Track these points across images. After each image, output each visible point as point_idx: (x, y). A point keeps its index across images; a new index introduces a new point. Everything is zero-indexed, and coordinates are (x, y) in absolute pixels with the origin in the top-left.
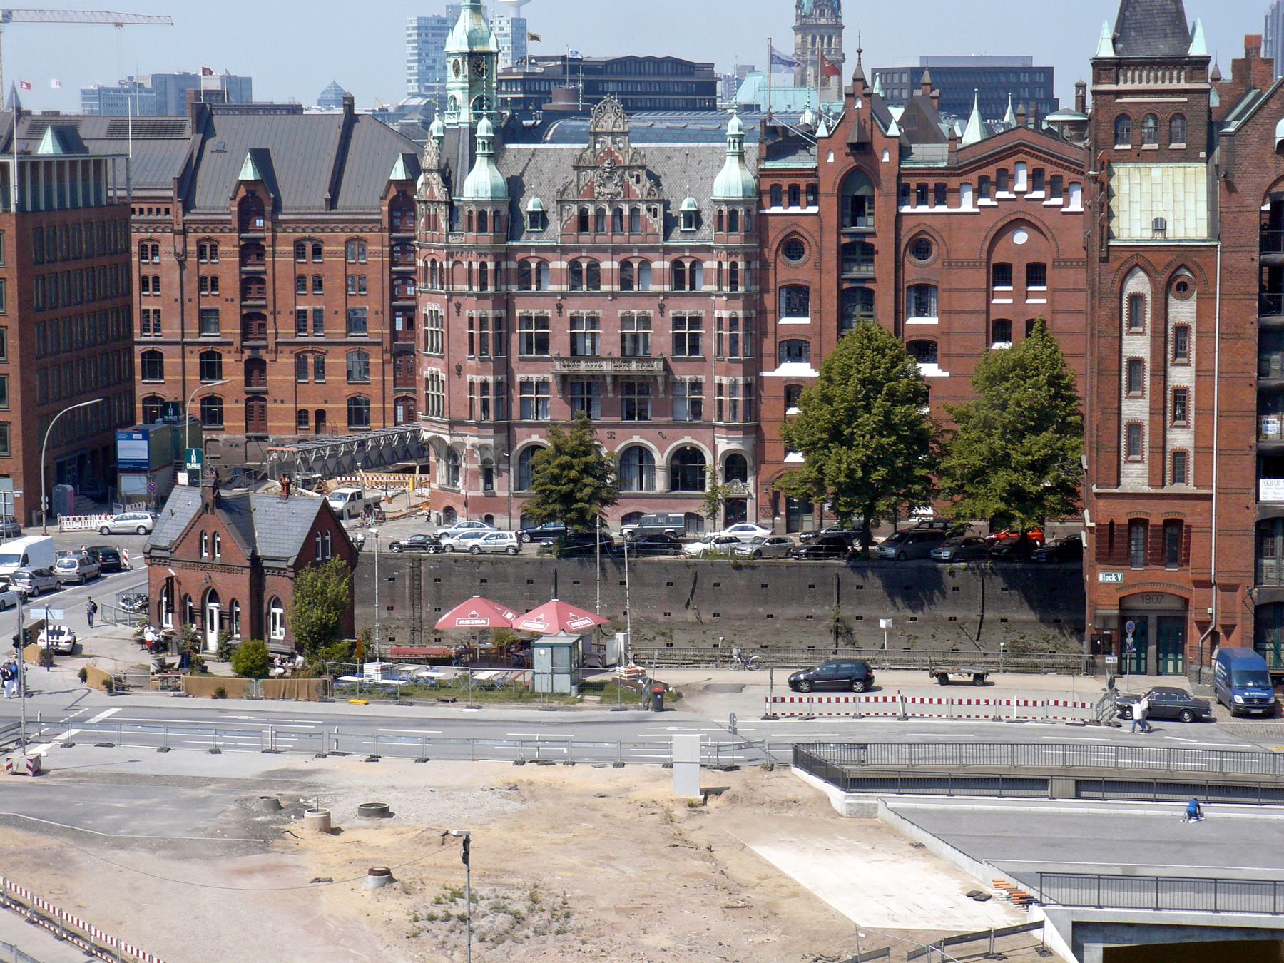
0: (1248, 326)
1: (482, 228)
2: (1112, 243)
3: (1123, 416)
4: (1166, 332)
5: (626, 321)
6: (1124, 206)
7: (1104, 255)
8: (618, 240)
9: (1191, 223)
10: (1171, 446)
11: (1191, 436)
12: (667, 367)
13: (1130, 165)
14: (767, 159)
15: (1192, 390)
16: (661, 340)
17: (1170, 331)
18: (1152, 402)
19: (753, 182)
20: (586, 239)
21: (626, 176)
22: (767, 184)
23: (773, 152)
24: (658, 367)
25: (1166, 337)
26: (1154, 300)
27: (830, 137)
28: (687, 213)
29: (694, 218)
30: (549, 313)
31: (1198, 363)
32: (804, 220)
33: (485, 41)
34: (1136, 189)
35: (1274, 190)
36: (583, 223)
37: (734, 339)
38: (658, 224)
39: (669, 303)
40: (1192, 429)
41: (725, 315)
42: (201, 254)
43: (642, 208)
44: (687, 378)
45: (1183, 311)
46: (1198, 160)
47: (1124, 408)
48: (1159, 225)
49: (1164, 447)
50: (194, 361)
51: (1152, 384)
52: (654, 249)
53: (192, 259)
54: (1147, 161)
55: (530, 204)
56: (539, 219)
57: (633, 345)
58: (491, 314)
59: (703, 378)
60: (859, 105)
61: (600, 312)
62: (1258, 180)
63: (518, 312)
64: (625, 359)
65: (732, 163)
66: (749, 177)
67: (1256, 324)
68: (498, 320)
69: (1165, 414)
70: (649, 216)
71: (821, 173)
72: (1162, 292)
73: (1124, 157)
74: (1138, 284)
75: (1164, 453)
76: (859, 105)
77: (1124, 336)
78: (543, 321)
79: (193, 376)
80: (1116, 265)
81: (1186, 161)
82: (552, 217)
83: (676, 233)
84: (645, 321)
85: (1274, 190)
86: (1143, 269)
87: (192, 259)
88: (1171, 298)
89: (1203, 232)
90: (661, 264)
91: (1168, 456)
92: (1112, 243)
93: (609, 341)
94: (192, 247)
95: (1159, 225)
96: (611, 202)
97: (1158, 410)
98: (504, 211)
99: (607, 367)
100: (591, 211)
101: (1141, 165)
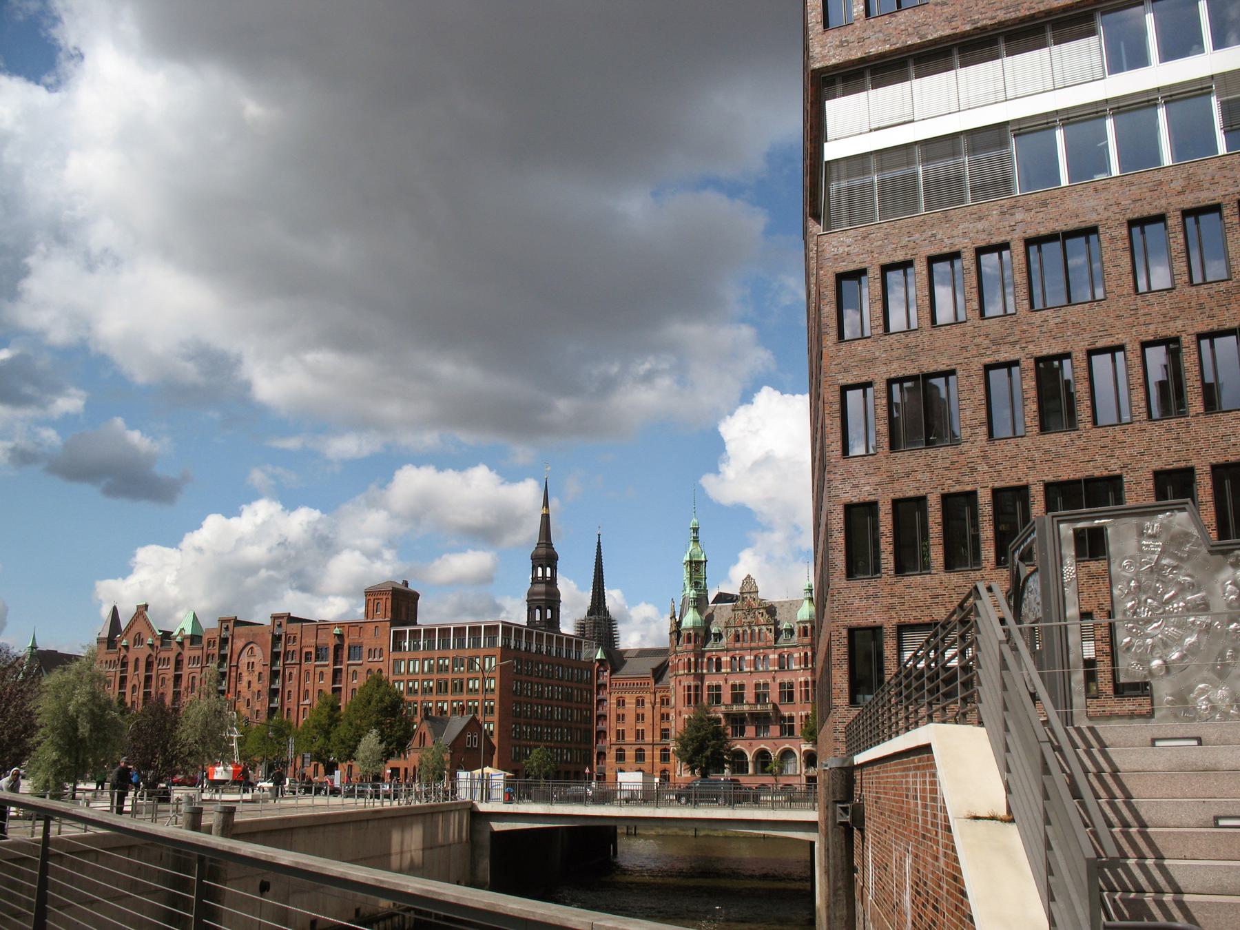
1: (689, 641)
5: (757, 686)
7: (1195, 743)
8: (753, 644)
12: (775, 706)
16: (774, 694)
20: (738, 645)
24: (770, 707)
29: (791, 631)
30: (721, 683)
33: (699, 556)
36: (737, 638)
37: (807, 691)
38: (771, 636)
39: (777, 675)
41: (803, 679)
42: (662, 703)
44: (787, 714)
50: (657, 753)
52: (770, 648)
53: (658, 705)
56: (719, 636)
57: (760, 697)
58: (692, 684)
59: (794, 714)
61: (745, 682)
63: (707, 683)
64: (755, 704)
68: (696, 687)
78: (718, 687)
79: (657, 760)
83: (781, 640)
84: (766, 685)
87: (658, 705)
90: (773, 656)
93: (749, 695)
94: (658, 700)
96: (750, 626)
98: (702, 633)
99: (746, 708)
100: (741, 630)
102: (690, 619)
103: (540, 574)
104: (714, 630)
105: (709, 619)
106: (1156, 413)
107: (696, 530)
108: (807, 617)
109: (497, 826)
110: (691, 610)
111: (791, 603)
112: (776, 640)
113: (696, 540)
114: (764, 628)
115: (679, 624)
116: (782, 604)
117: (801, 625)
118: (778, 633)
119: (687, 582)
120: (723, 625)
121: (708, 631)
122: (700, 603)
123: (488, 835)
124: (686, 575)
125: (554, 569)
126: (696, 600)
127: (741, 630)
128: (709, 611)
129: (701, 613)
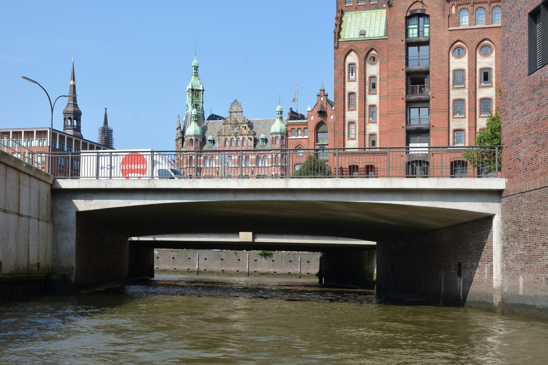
0: (401, 71)
2: (339, 40)
3: (346, 119)
4: (365, 79)
6: (348, 27)
9: (377, 31)
10: (368, 132)
11: (378, 127)
13: (352, 12)
14: (290, 120)
15: (378, 105)
17: (367, 79)
18: (360, 111)
19: (284, 128)
21: (241, 127)
22: (289, 128)
23: (292, 118)
25: (365, 82)
26: (360, 65)
27: (312, 111)
28: (262, 139)
29: (266, 140)
31: (380, 93)
32: (303, 141)
34: (354, 21)
35: (411, 9)
38: (252, 143)
40: (378, 123)
43: (246, 137)
45: (373, 70)
46: (383, 8)
47: (346, 115)
48: (363, 33)
49: (365, 132)
51: (359, 103)
54: (360, 10)
55: (209, 137)
60: (322, 98)
62: (404, 4)
65: (278, 121)
66: (284, 127)
67: (404, 70)
69: (365, 117)
70: (249, 140)
71: (308, 124)
72: (363, 63)
73: (350, 9)
74: (352, 58)
75: (365, 135)
76: (322, 98)
77: (346, 83)
80: (342, 50)
81: (377, 9)
82: (216, 141)
85: (411, 9)
86: (355, 52)
88: (367, 64)
89: (382, 34)
91: (367, 136)
92: (339, 40)
95: (363, 33)
96: (236, 136)
97: (363, 116)
98: (200, 139)
101: (357, 12)
102: (192, 129)
103: (69, 124)
104: (209, 137)
105: (204, 130)
106: (490, 85)
107: (196, 68)
108: (278, 130)
109: (83, 205)
110: (193, 123)
111: (266, 122)
112: (255, 145)
113: (196, 75)
114: (246, 137)
115: (183, 132)
116: (259, 122)
117: (274, 136)
118: (256, 141)
119: (190, 104)
120: (216, 134)
121: (204, 139)
122: (199, 118)
123: (74, 215)
124: (188, 100)
125: (79, 121)
126: (197, 116)
127: (229, 138)
128: (205, 124)
129: (199, 125)
